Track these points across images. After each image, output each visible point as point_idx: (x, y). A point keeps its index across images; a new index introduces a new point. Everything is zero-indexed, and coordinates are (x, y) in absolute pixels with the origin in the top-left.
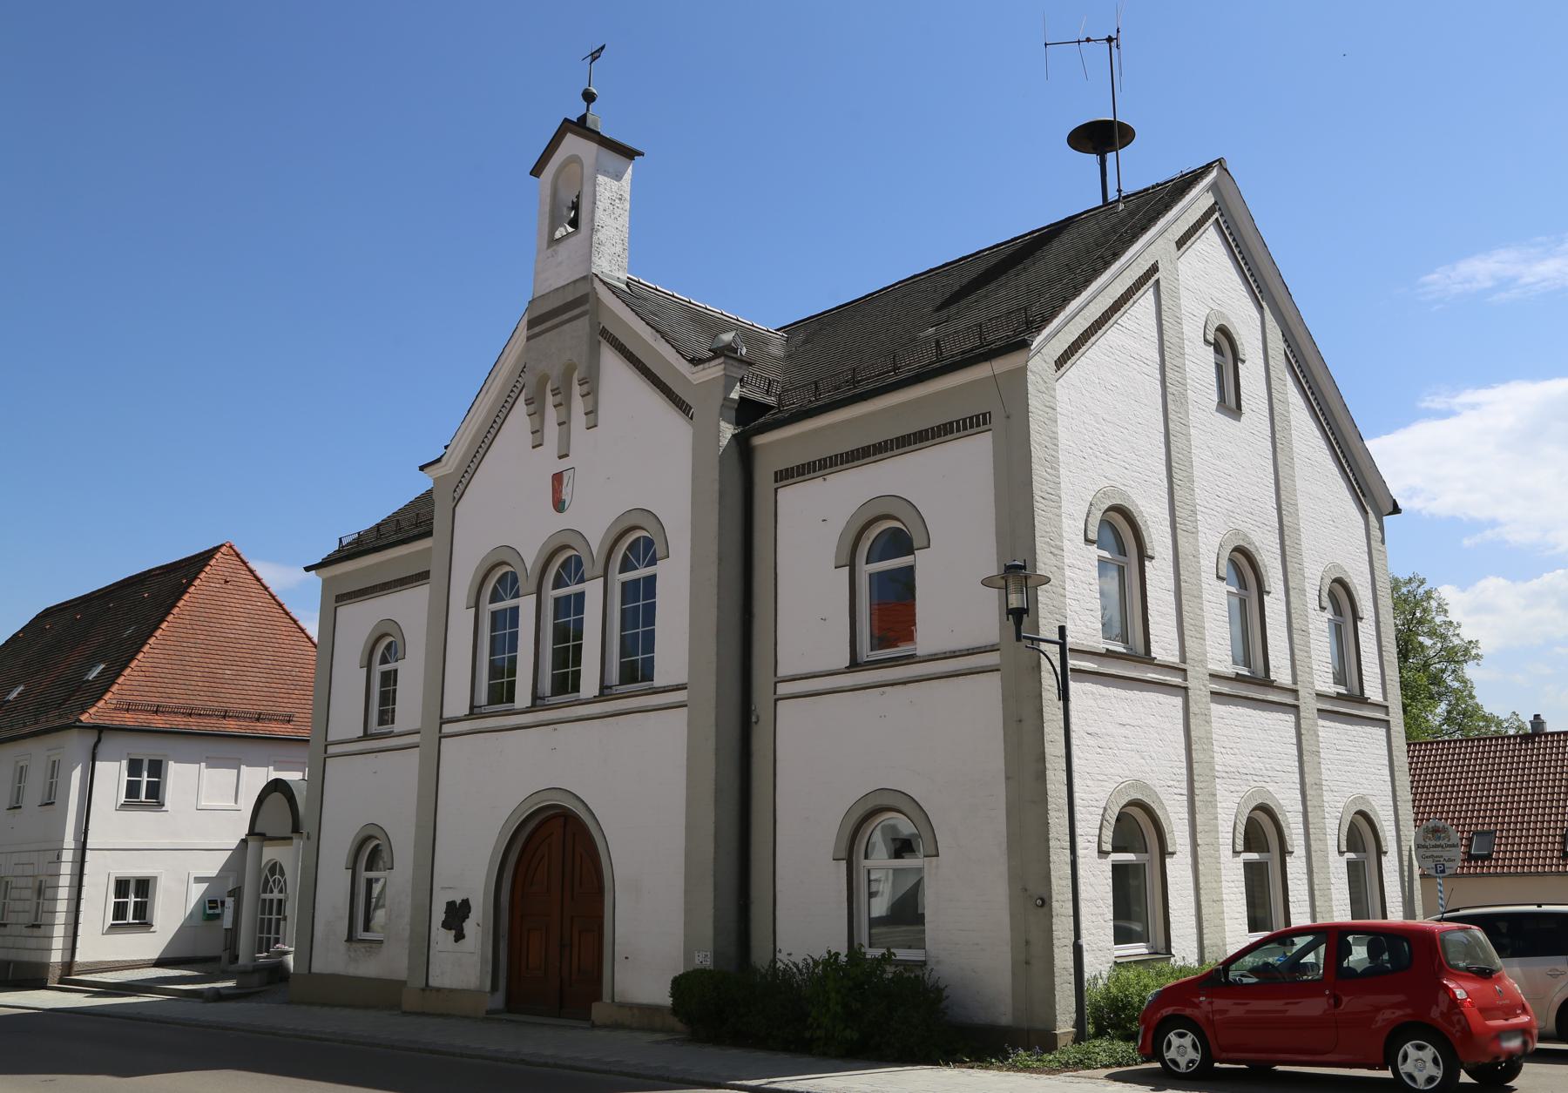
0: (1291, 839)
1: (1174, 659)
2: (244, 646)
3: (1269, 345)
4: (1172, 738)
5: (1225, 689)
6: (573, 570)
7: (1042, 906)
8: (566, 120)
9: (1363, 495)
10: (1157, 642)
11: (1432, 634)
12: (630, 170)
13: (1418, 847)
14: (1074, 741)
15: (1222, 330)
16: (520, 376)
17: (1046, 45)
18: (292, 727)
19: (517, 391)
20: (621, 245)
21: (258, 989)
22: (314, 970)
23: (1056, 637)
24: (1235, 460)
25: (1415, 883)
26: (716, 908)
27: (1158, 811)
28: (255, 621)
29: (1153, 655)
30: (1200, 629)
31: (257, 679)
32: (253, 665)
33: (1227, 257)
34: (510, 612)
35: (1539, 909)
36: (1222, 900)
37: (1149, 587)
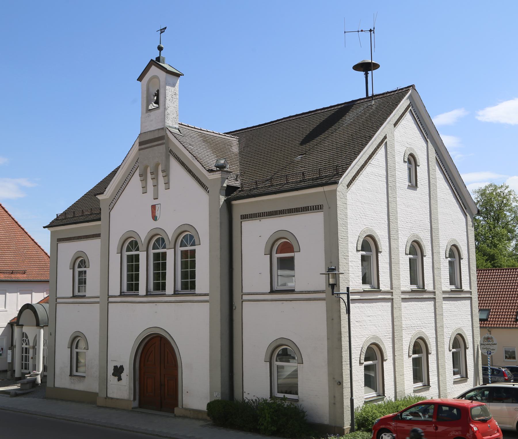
0: (431, 348)
1: (388, 289)
2: (4, 241)
3: (430, 156)
4: (387, 318)
5: (407, 296)
6: (161, 242)
7: (340, 385)
8: (152, 60)
9: (466, 209)
10: (382, 283)
11: (510, 210)
12: (178, 82)
13: (481, 344)
14: (352, 325)
15: (412, 155)
16: (136, 163)
17: (345, 32)
18: (26, 275)
19: (135, 169)
20: (176, 114)
21: (30, 390)
22: (57, 385)
23: (346, 292)
24: (414, 206)
25: (479, 358)
26: (221, 377)
27: (381, 346)
28: (7, 230)
29: (381, 288)
30: (398, 276)
31: (10, 256)
32: (8, 249)
33: (414, 124)
34: (135, 256)
35: (514, 386)
36: (404, 375)
37: (379, 263)
